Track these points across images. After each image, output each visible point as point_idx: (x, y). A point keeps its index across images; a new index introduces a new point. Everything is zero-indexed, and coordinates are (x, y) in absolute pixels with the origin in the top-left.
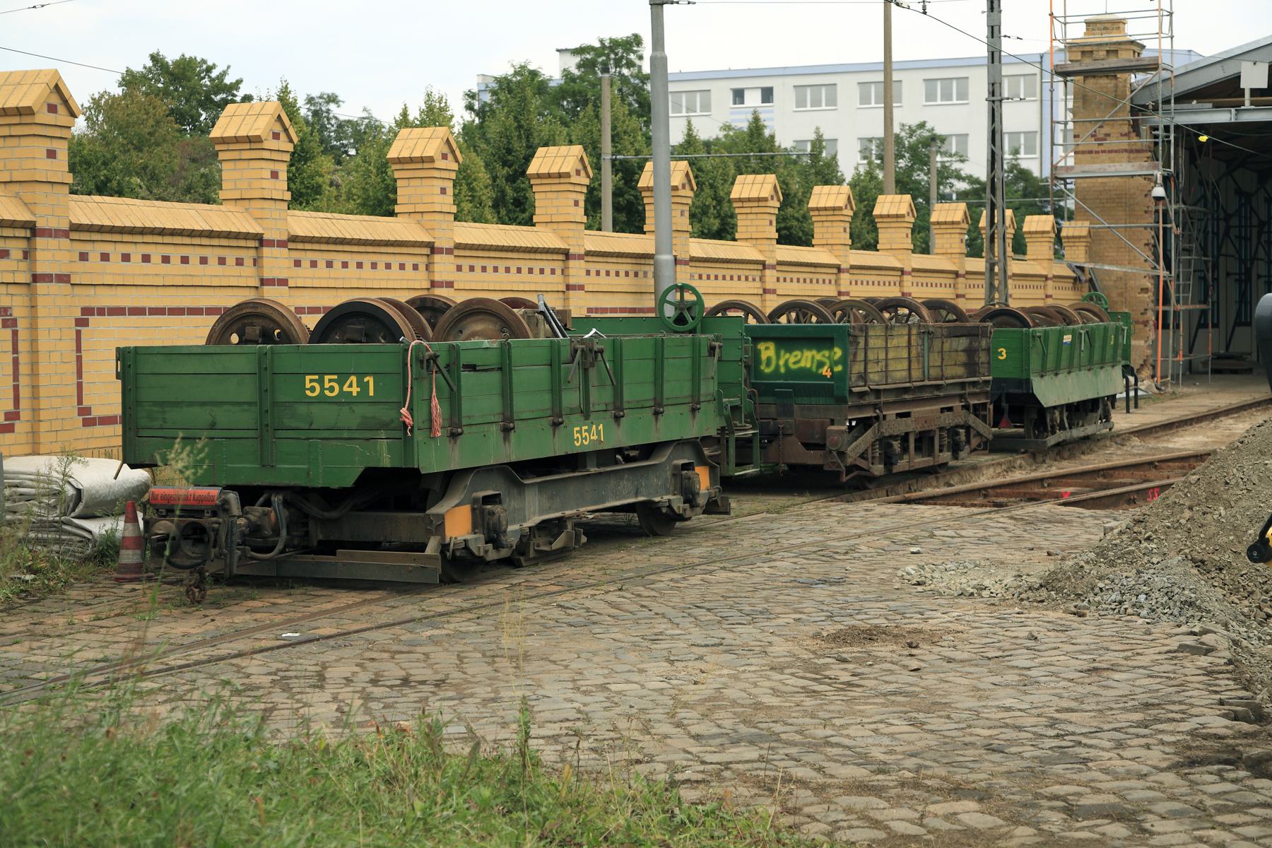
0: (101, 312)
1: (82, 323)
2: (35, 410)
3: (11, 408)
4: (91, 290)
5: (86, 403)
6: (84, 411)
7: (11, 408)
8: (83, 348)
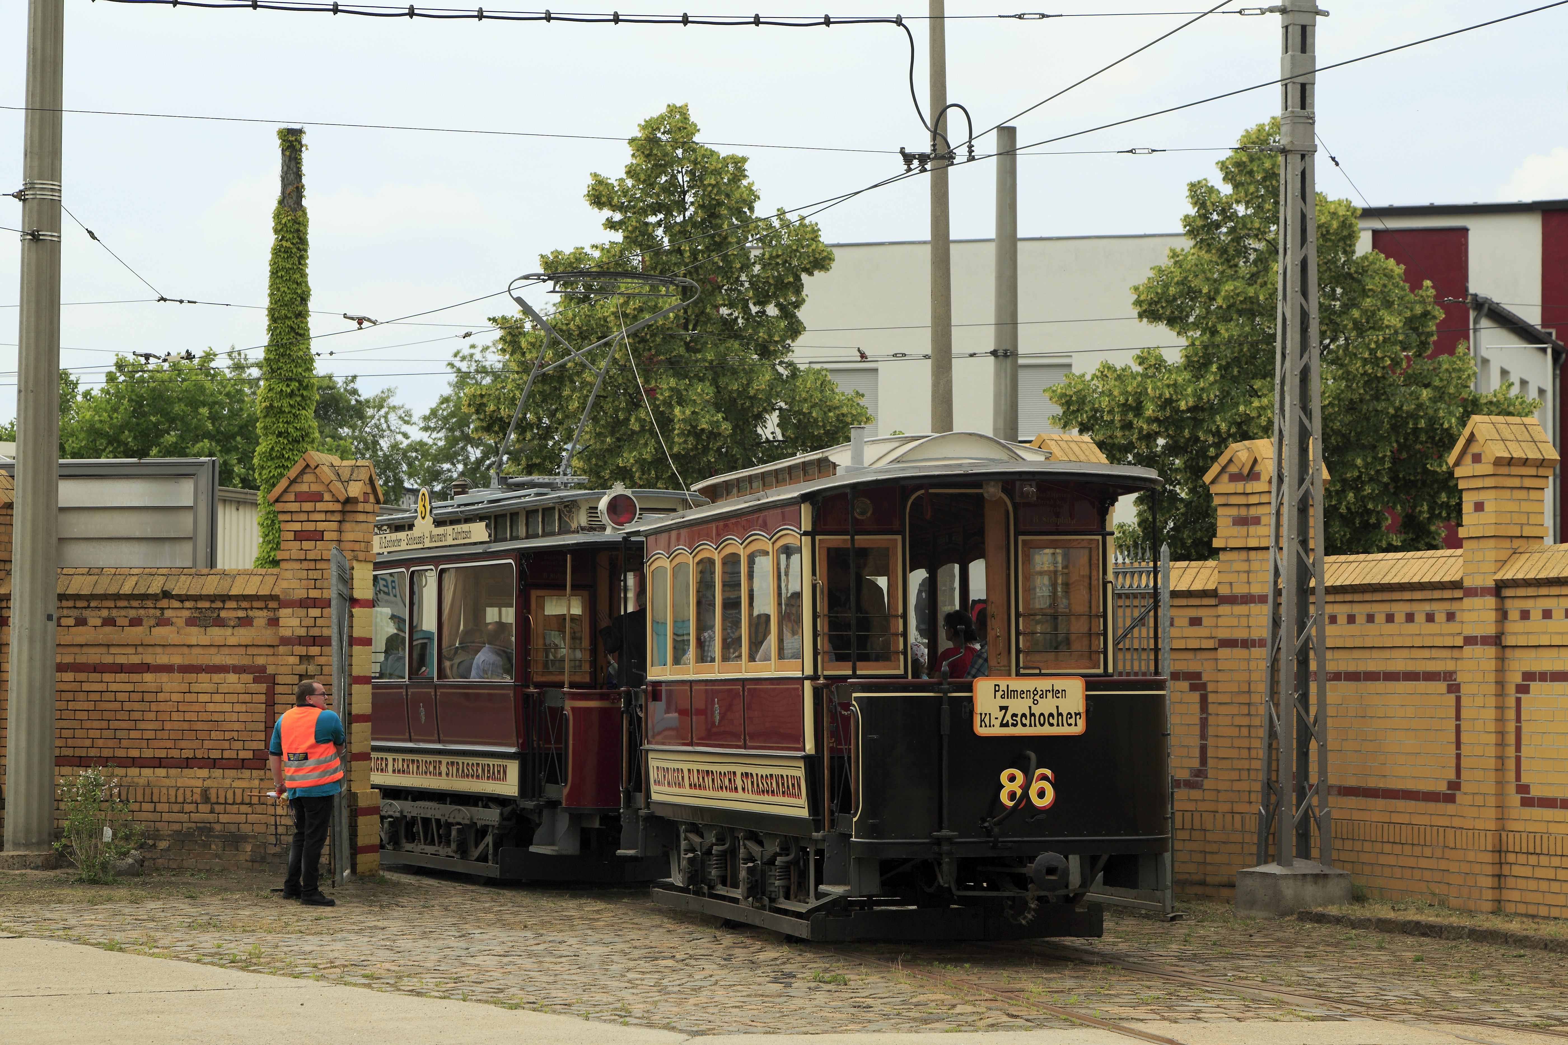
0: (1543, 677)
1: (1455, 786)
2: (1501, 694)
3: (1452, 776)
4: (1532, 653)
5: (1524, 780)
6: (1454, 689)
7: (1452, 776)
8: (1523, 718)
